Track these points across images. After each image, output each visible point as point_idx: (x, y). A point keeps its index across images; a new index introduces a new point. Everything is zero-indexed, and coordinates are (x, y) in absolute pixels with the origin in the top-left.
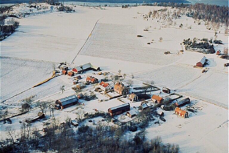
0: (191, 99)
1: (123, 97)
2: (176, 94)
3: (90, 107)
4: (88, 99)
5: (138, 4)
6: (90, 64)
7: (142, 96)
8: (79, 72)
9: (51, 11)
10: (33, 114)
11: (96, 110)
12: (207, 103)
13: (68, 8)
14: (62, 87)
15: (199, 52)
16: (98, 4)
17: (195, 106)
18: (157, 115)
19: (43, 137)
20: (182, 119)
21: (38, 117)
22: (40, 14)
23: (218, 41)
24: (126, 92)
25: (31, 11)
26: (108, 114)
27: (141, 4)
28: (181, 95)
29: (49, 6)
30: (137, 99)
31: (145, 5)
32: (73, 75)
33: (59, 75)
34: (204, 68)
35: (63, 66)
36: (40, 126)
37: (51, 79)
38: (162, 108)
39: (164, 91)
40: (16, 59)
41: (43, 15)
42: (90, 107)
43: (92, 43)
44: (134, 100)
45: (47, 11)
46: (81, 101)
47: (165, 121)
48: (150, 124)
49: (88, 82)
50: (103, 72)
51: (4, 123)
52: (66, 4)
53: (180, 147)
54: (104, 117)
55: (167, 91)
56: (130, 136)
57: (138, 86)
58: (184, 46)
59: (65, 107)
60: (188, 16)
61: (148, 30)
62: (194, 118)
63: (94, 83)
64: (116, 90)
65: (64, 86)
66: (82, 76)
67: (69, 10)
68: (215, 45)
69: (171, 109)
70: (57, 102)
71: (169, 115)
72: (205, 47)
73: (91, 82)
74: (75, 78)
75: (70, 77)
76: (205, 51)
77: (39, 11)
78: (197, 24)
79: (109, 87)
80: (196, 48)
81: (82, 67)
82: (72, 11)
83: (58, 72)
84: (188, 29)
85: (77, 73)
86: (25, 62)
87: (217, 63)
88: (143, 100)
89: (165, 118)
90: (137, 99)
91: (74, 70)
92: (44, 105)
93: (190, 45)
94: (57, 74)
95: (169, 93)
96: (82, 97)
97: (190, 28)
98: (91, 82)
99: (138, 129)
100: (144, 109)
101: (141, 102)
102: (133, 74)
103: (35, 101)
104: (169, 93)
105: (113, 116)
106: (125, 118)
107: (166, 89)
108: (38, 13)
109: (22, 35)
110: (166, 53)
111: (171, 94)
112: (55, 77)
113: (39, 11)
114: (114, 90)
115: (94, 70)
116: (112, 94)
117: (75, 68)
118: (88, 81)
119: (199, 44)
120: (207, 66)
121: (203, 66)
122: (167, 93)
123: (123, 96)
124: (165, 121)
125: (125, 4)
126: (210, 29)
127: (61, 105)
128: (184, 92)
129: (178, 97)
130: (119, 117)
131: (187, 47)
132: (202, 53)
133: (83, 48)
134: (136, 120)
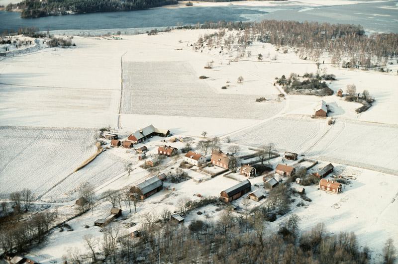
0: (334, 165)
1: (231, 172)
2: (307, 160)
3: (188, 191)
4: (176, 180)
5: (171, 27)
6: (151, 127)
7: (260, 169)
8: (141, 141)
9: (38, 47)
10: (101, 212)
11: (199, 196)
12: (357, 169)
13: (64, 42)
14: (127, 165)
15: (310, 95)
16: (105, 32)
17: (345, 174)
18: (296, 194)
19: (136, 245)
20: (335, 197)
21: (113, 216)
22: (22, 55)
23: (328, 76)
24: (233, 164)
25: (6, 50)
26: (221, 200)
27: (174, 27)
28: (316, 161)
29: (33, 40)
30: (254, 173)
31: (181, 28)
32: (132, 146)
33: (109, 149)
34: (329, 118)
35: (106, 133)
36: (122, 230)
37: (98, 155)
38: (298, 182)
39: (287, 157)
40: (25, 129)
41: (28, 56)
42: (188, 191)
43: (133, 94)
44: (251, 175)
45: (32, 48)
46: (166, 184)
47: (310, 201)
48: (291, 208)
49: (161, 154)
50: (177, 137)
51: (60, 231)
52: (57, 35)
53: (356, 233)
54: (218, 205)
55: (293, 157)
56: (274, 227)
57: (244, 153)
58: (281, 89)
59: (147, 195)
60: (262, 41)
61: (211, 68)
62: (349, 192)
63: (173, 155)
64: (216, 163)
65: (131, 164)
66: (147, 145)
67: (66, 45)
68: (327, 82)
69: (312, 182)
70: (133, 190)
71: (312, 191)
72: (315, 87)
73: (166, 155)
74: (138, 151)
75: (128, 150)
76: (317, 92)
77: (19, 49)
78: (282, 52)
79: (202, 160)
80: (303, 89)
81: (142, 133)
82: (72, 46)
83: (104, 144)
84: (273, 61)
85: (137, 142)
86: (41, 133)
87: (343, 109)
88: (267, 173)
89: (308, 196)
90: (254, 173)
91: (131, 137)
92: (111, 195)
93: (292, 85)
94: (104, 146)
95: (296, 159)
96: (164, 179)
97: (276, 60)
98: (166, 155)
99: (277, 216)
100: (274, 186)
101: (79, 206)
102: (229, 135)
103: (99, 191)
104: (296, 159)
105: (231, 202)
106: (248, 204)
107: (291, 155)
108: (20, 52)
109: (11, 89)
110: (260, 100)
111: (299, 160)
112: (103, 151)
113: (19, 49)
114: (212, 163)
115: (161, 135)
116: (214, 170)
117: (133, 135)
118: (161, 152)
119: (305, 83)
120: (330, 114)
121: (327, 116)
122: (294, 160)
123: (231, 171)
124: (310, 201)
125: (150, 29)
126: (305, 59)
127: (138, 195)
128: (318, 156)
129: (312, 164)
130: (240, 202)
131: (288, 88)
132: (314, 96)
133: (122, 104)
134: (265, 203)
